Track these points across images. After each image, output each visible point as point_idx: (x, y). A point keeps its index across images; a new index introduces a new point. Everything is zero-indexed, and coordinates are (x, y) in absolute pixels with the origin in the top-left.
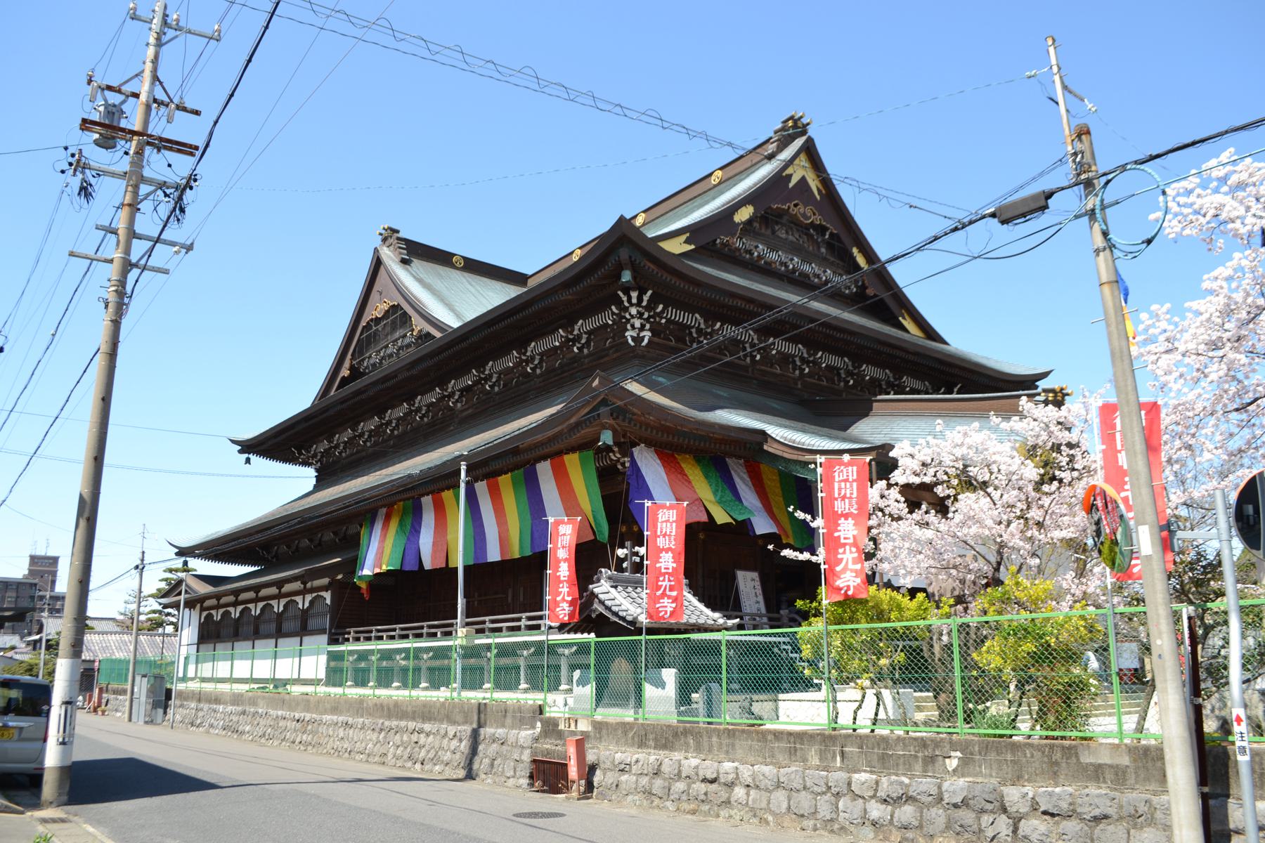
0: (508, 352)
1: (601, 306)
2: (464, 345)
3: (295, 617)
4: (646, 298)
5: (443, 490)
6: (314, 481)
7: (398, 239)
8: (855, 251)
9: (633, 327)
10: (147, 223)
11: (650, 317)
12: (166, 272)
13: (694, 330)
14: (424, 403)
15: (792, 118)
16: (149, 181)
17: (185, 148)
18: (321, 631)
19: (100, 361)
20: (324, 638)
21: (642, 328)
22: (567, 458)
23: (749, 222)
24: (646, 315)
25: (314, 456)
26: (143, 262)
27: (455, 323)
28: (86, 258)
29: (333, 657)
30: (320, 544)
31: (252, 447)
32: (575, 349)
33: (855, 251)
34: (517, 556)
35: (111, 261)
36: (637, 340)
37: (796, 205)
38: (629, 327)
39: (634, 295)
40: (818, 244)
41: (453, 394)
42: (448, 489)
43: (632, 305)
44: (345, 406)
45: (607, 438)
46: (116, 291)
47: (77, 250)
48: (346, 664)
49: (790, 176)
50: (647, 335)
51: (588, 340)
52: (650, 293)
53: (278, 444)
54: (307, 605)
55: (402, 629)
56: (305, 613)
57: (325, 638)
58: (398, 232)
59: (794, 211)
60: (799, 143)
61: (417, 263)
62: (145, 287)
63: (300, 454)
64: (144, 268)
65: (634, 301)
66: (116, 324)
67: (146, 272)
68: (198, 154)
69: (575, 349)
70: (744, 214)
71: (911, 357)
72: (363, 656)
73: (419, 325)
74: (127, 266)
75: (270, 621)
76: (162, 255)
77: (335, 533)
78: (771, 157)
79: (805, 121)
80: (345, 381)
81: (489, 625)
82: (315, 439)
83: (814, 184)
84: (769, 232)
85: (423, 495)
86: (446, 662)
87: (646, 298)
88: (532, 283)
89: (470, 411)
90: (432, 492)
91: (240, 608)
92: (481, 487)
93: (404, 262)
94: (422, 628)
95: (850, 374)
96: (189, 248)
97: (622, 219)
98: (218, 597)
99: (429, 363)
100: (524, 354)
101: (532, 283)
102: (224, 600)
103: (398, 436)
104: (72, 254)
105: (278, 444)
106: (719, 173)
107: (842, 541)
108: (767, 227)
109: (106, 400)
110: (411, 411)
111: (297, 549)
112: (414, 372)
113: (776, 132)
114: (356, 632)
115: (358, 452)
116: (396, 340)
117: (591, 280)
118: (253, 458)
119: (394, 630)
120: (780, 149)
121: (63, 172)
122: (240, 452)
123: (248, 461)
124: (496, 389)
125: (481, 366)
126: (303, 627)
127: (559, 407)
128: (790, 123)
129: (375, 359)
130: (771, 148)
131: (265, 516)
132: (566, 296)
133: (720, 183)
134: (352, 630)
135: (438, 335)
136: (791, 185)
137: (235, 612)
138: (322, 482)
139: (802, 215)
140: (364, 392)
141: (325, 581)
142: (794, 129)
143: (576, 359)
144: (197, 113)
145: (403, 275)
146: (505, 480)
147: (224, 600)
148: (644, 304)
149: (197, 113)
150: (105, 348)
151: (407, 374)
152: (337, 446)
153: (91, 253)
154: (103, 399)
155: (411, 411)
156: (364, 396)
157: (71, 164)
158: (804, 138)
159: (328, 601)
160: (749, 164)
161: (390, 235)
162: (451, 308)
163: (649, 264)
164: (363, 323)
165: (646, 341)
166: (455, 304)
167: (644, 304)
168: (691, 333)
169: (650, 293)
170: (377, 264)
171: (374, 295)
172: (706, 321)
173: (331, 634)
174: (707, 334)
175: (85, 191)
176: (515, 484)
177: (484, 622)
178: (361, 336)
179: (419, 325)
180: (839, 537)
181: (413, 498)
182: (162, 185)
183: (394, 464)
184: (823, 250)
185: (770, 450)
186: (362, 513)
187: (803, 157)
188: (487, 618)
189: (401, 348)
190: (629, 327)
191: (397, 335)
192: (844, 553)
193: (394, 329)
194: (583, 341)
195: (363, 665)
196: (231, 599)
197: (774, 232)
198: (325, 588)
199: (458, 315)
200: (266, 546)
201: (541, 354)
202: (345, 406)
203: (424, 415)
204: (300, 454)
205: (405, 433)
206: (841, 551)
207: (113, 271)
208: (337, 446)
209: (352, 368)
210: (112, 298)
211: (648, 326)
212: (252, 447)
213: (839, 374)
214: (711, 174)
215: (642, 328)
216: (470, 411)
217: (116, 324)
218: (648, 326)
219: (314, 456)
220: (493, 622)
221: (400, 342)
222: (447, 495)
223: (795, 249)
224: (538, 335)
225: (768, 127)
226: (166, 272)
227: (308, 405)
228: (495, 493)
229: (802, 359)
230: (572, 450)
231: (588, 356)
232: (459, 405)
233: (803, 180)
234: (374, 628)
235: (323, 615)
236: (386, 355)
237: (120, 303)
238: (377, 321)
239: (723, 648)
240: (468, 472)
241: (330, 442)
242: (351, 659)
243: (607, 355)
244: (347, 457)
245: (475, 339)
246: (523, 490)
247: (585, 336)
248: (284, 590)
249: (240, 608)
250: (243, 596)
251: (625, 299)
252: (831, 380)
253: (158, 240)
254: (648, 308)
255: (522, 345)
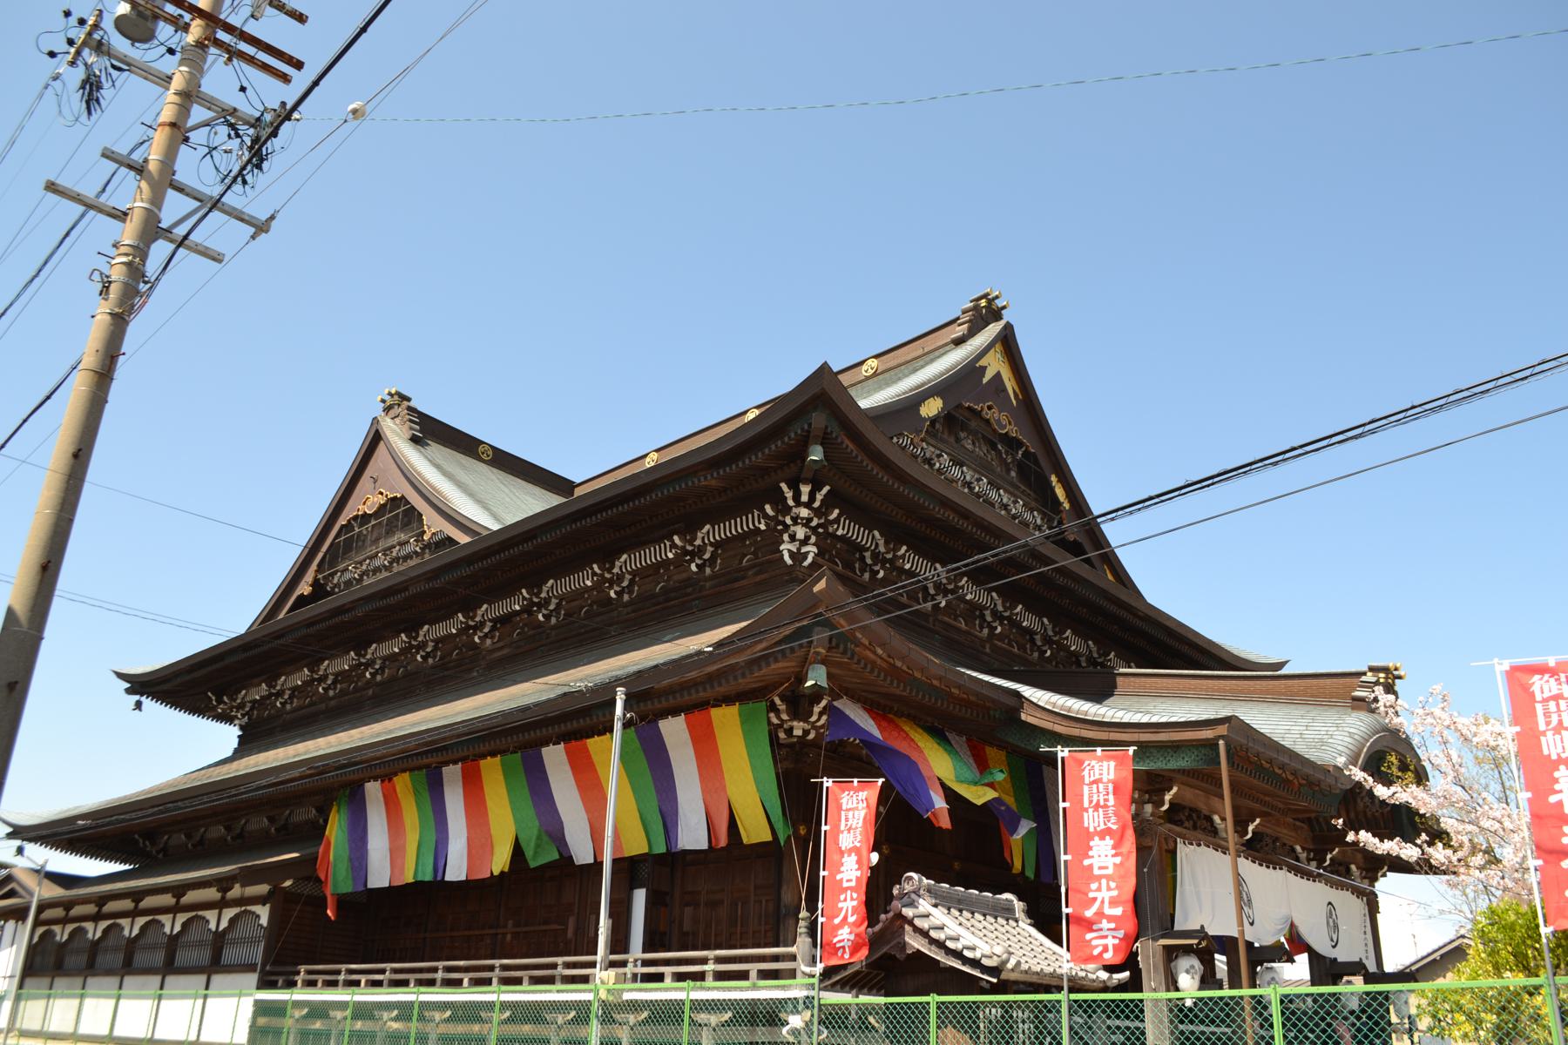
0: (450, 615)
1: (750, 503)
2: (528, 547)
3: (200, 944)
4: (819, 497)
5: (484, 756)
6: (235, 743)
7: (410, 409)
8: (1054, 479)
9: (793, 538)
10: (192, 168)
11: (819, 526)
12: (217, 258)
13: (868, 554)
14: (289, 685)
15: (985, 296)
16: (209, 103)
17: (280, 63)
18: (248, 968)
19: (78, 388)
20: (253, 978)
21: (805, 542)
22: (715, 713)
23: (933, 421)
24: (814, 523)
25: (241, 706)
26: (181, 231)
27: (495, 527)
28: (76, 198)
29: (261, 1009)
30: (240, 836)
31: (145, 686)
32: (693, 567)
33: (1054, 479)
34: (411, 880)
35: (122, 216)
36: (798, 557)
37: (990, 408)
38: (786, 537)
39: (805, 489)
40: (1007, 464)
41: (482, 624)
42: (493, 754)
43: (798, 503)
44: (312, 630)
45: (816, 677)
46: (129, 265)
47: (64, 182)
48: (288, 1023)
49: (984, 368)
50: (811, 550)
51: (714, 556)
52: (826, 489)
53: (185, 686)
54: (177, 928)
55: (395, 971)
56: (220, 938)
57: (253, 978)
58: (409, 400)
59: (988, 414)
60: (993, 329)
61: (435, 449)
62: (179, 282)
63: (220, 701)
64: (182, 243)
65: (805, 498)
66: (119, 322)
67: (215, 214)
68: (301, 80)
69: (693, 567)
70: (932, 408)
71: (1139, 623)
72: (319, 1011)
73: (434, 525)
74: (152, 230)
75: (153, 947)
76: (216, 231)
77: (271, 820)
78: (959, 342)
79: (999, 303)
80: (302, 601)
81: (561, 971)
82: (247, 681)
83: (1010, 384)
84: (952, 440)
85: (447, 763)
86: (476, 1028)
87: (819, 497)
88: (578, 492)
89: (505, 651)
90: (463, 759)
91: (104, 924)
92: (674, 730)
93: (415, 440)
94: (435, 970)
95: (1047, 640)
96: (261, 227)
97: (824, 369)
98: (68, 905)
99: (465, 571)
100: (473, 618)
101: (578, 492)
102: (77, 911)
103: (381, 683)
104: (51, 187)
105: (185, 686)
106: (874, 363)
107: (1096, 872)
108: (950, 433)
109: (80, 457)
110: (271, 695)
111: (201, 842)
112: (437, 584)
113: (964, 312)
114: (309, 972)
115: (312, 704)
116: (361, 563)
117: (757, 458)
118: (147, 702)
119: (383, 971)
120: (973, 332)
121: (52, 54)
122: (128, 691)
123: (139, 705)
124: (553, 620)
125: (535, 584)
126: (211, 961)
127: (703, 641)
128: (983, 303)
129: (353, 573)
130: (959, 330)
131: (168, 785)
132: (710, 480)
133: (875, 374)
134: (303, 968)
135: (463, 539)
136: (985, 380)
137: (94, 931)
138: (246, 745)
139: (997, 419)
140: (348, 611)
141: (263, 889)
142: (985, 312)
143: (691, 581)
144: (301, 18)
145: (415, 458)
146: (403, 782)
147: (77, 911)
148: (816, 504)
149: (301, 18)
150: (90, 360)
151: (422, 587)
152: (280, 694)
153: (89, 191)
154: (76, 456)
155: (412, 647)
156: (346, 617)
157: (71, 42)
158: (1001, 324)
159: (264, 921)
160: (920, 352)
161: (398, 401)
162: (486, 507)
163: (847, 442)
164: (342, 521)
165: (810, 559)
166: (490, 507)
167: (816, 504)
168: (863, 559)
169: (826, 489)
170: (375, 439)
171: (365, 482)
172: (886, 543)
173: (263, 974)
174: (885, 561)
175: (91, 89)
176: (507, 772)
177: (554, 966)
178: (336, 539)
179: (434, 525)
180: (1091, 866)
181: (428, 766)
182: (229, 117)
183: (516, 682)
184: (1013, 474)
185: (1030, 720)
186: (340, 785)
187: (998, 347)
188: (560, 960)
189: (396, 560)
190: (786, 537)
191: (394, 540)
192: (1099, 889)
193: (390, 532)
194: (552, 607)
195: (318, 1025)
196: (91, 909)
197: (958, 440)
198: (261, 900)
199: (496, 518)
200: (151, 833)
201: (634, 573)
202: (312, 630)
203: (486, 636)
204: (220, 701)
205: (393, 679)
206: (1094, 886)
207: (128, 233)
208: (280, 694)
209: (316, 584)
210: (117, 274)
211: (813, 539)
212: (145, 686)
213: (1033, 641)
214: (645, 456)
215: (805, 542)
216: (505, 651)
217: (119, 322)
218: (813, 539)
219: (241, 706)
220: (568, 965)
221: (395, 551)
222: (593, 743)
223: (982, 468)
224: (635, 543)
225: (958, 303)
226: (217, 258)
227: (243, 631)
228: (705, 744)
229: (995, 613)
230: (728, 700)
231: (712, 578)
232: (489, 642)
233: (998, 375)
234: (343, 967)
235: (252, 941)
236: (376, 566)
237: (132, 292)
238: (365, 518)
239: (687, 1010)
240: (626, 708)
241: (270, 686)
242: (297, 1014)
243: (744, 578)
244: (294, 710)
245: (547, 538)
246: (426, 796)
247: (554, 601)
248: (185, 900)
249: (70, 928)
250: (111, 906)
251: (789, 494)
252: (1022, 647)
253: (216, 204)
254: (818, 512)
255: (607, 557)
